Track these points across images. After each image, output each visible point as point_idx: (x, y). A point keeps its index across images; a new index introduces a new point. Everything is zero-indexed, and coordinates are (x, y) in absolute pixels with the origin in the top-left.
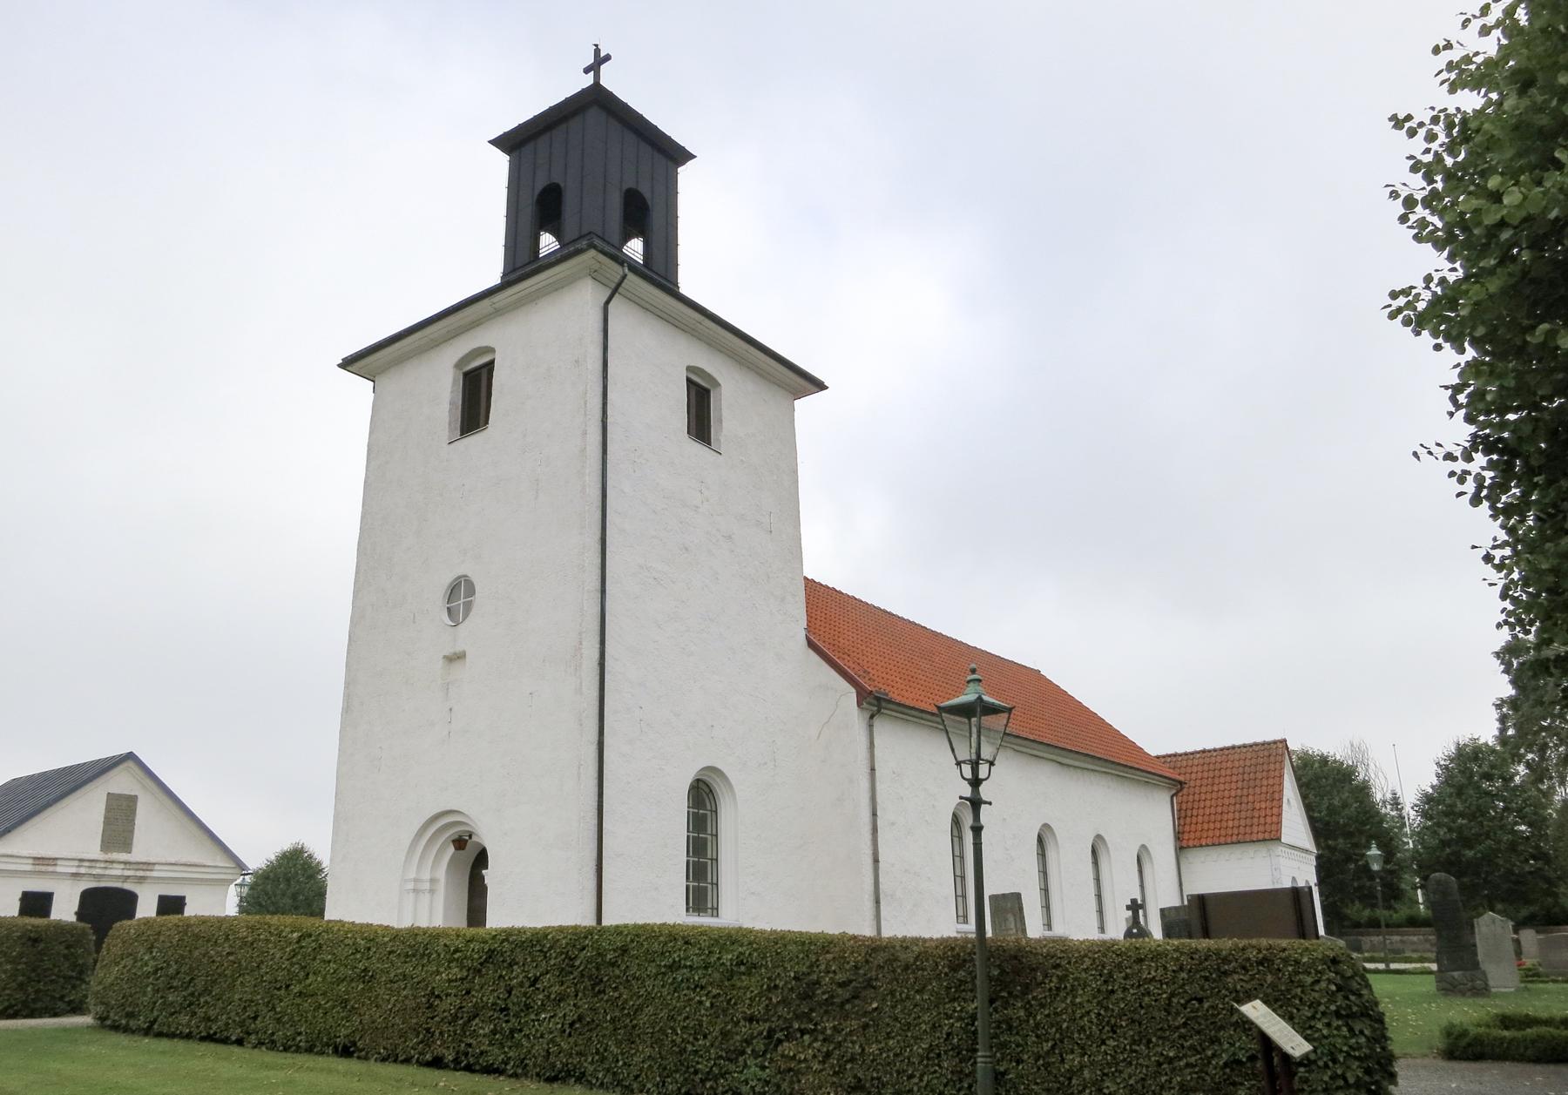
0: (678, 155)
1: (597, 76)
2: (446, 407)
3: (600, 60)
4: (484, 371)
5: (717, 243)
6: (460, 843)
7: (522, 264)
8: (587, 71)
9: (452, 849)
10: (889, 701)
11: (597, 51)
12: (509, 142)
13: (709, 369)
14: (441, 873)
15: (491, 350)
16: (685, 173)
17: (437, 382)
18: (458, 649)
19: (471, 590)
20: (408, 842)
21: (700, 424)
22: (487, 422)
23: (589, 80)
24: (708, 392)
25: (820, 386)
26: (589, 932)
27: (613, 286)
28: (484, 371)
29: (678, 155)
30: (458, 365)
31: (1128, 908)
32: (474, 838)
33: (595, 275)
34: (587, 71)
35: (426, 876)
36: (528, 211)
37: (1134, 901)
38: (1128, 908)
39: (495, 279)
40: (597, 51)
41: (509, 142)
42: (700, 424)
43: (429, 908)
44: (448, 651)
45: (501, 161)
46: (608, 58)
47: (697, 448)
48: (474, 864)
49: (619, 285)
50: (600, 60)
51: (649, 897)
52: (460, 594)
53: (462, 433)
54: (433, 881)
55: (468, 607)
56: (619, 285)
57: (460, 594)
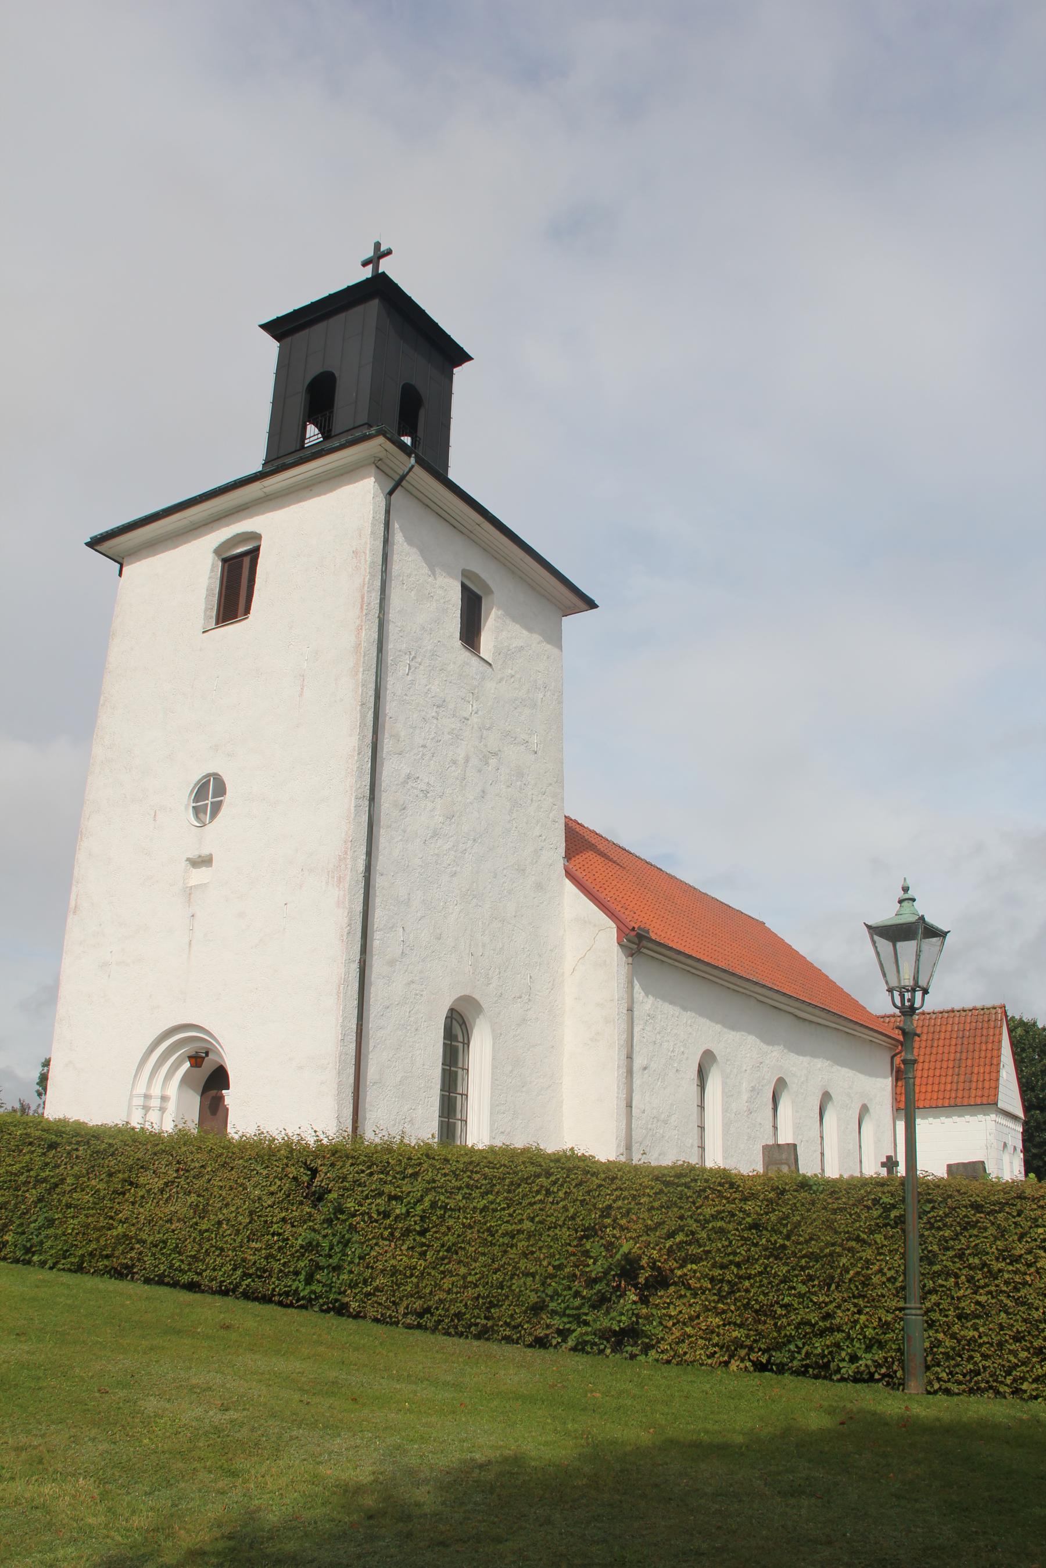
0: (455, 356)
1: (376, 267)
2: (203, 593)
3: (380, 254)
4: (247, 561)
5: (485, 437)
6: (197, 1060)
7: (284, 453)
8: (365, 264)
9: (188, 1064)
10: (651, 940)
11: (377, 245)
12: (279, 328)
13: (484, 575)
14: (173, 1089)
15: (258, 537)
16: (461, 374)
17: (192, 567)
18: (205, 852)
19: (221, 789)
20: (134, 1072)
21: (470, 633)
22: (247, 611)
23: (367, 273)
24: (479, 599)
25: (591, 605)
26: (334, 1153)
27: (397, 478)
28: (247, 561)
29: (455, 356)
30: (217, 551)
31: (883, 1165)
32: (211, 1056)
33: (379, 466)
34: (365, 264)
35: (156, 1091)
36: (298, 403)
37: (889, 1158)
38: (883, 1165)
39: (257, 467)
40: (377, 245)
41: (279, 328)
42: (470, 633)
43: (164, 1108)
44: (193, 854)
45: (271, 347)
46: (389, 252)
47: (465, 655)
48: (213, 1082)
49: (403, 478)
50: (380, 254)
51: (402, 1115)
52: (209, 795)
53: (217, 623)
54: (164, 1098)
55: (217, 808)
56: (403, 478)
57: (209, 795)
